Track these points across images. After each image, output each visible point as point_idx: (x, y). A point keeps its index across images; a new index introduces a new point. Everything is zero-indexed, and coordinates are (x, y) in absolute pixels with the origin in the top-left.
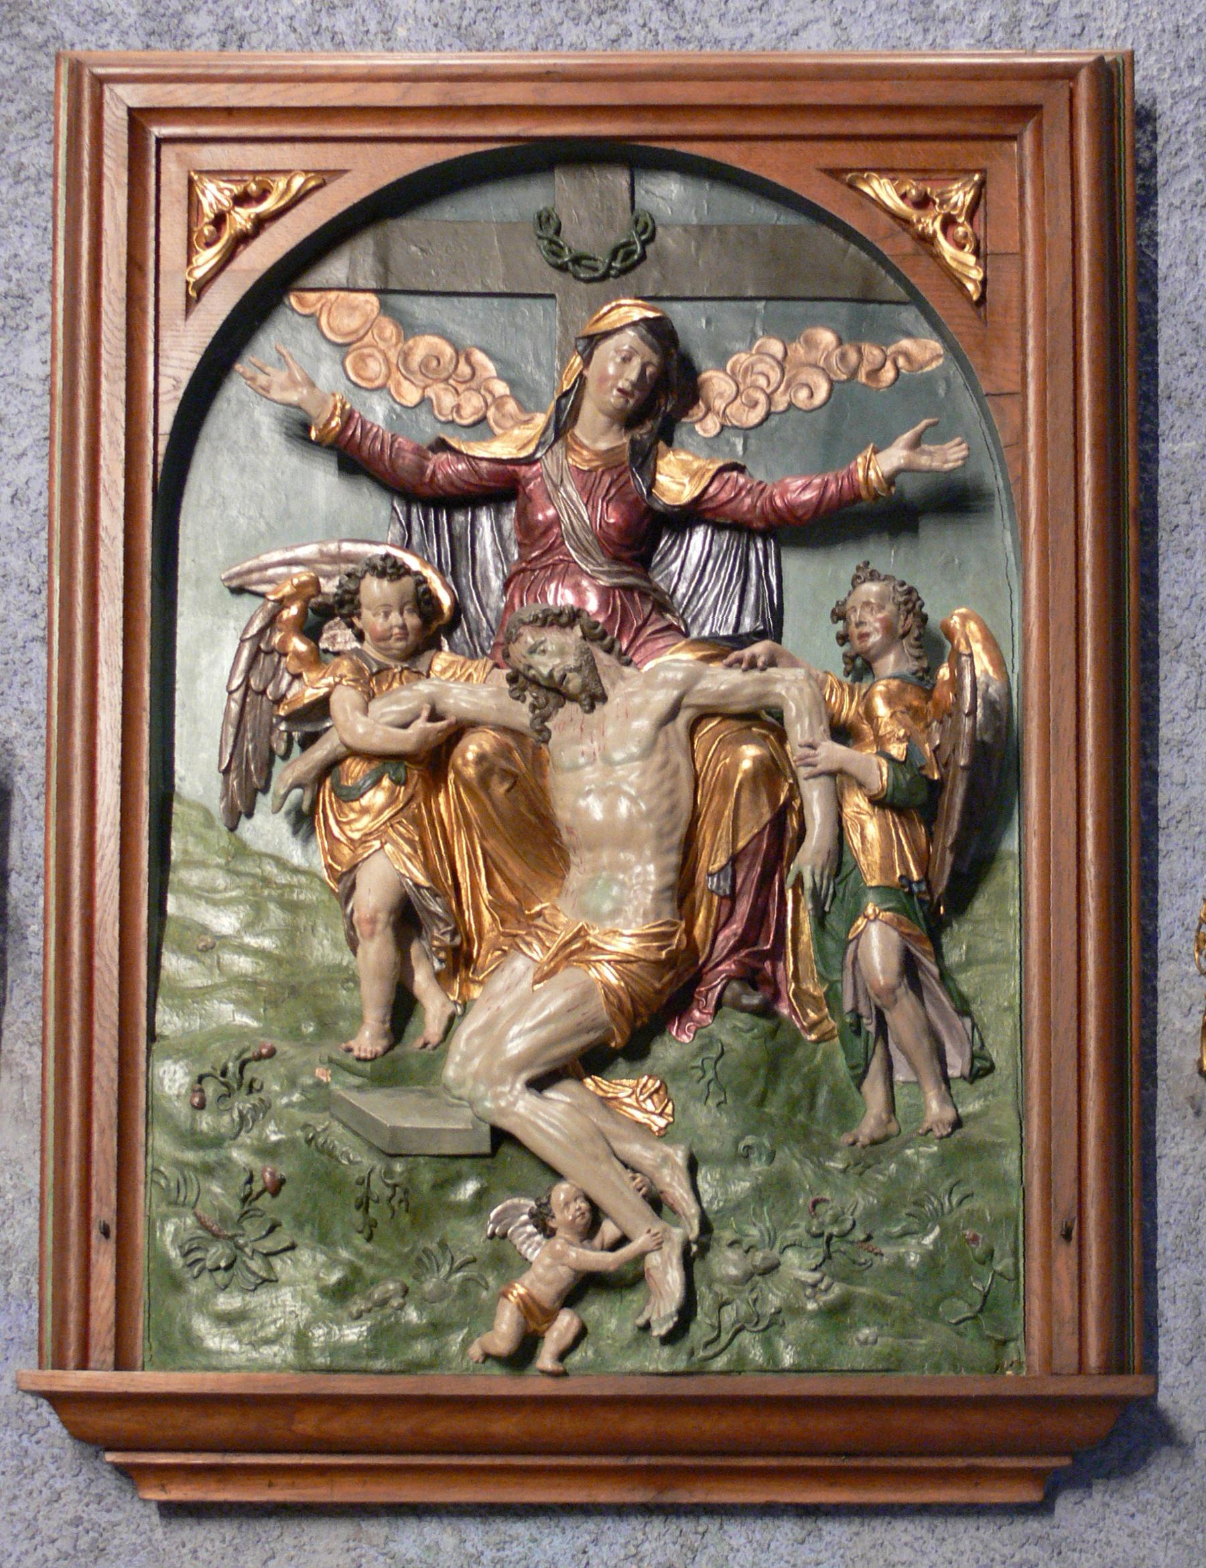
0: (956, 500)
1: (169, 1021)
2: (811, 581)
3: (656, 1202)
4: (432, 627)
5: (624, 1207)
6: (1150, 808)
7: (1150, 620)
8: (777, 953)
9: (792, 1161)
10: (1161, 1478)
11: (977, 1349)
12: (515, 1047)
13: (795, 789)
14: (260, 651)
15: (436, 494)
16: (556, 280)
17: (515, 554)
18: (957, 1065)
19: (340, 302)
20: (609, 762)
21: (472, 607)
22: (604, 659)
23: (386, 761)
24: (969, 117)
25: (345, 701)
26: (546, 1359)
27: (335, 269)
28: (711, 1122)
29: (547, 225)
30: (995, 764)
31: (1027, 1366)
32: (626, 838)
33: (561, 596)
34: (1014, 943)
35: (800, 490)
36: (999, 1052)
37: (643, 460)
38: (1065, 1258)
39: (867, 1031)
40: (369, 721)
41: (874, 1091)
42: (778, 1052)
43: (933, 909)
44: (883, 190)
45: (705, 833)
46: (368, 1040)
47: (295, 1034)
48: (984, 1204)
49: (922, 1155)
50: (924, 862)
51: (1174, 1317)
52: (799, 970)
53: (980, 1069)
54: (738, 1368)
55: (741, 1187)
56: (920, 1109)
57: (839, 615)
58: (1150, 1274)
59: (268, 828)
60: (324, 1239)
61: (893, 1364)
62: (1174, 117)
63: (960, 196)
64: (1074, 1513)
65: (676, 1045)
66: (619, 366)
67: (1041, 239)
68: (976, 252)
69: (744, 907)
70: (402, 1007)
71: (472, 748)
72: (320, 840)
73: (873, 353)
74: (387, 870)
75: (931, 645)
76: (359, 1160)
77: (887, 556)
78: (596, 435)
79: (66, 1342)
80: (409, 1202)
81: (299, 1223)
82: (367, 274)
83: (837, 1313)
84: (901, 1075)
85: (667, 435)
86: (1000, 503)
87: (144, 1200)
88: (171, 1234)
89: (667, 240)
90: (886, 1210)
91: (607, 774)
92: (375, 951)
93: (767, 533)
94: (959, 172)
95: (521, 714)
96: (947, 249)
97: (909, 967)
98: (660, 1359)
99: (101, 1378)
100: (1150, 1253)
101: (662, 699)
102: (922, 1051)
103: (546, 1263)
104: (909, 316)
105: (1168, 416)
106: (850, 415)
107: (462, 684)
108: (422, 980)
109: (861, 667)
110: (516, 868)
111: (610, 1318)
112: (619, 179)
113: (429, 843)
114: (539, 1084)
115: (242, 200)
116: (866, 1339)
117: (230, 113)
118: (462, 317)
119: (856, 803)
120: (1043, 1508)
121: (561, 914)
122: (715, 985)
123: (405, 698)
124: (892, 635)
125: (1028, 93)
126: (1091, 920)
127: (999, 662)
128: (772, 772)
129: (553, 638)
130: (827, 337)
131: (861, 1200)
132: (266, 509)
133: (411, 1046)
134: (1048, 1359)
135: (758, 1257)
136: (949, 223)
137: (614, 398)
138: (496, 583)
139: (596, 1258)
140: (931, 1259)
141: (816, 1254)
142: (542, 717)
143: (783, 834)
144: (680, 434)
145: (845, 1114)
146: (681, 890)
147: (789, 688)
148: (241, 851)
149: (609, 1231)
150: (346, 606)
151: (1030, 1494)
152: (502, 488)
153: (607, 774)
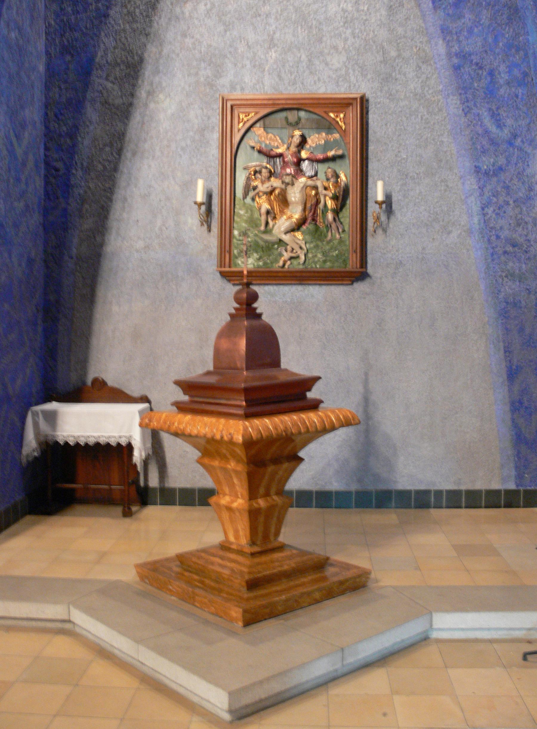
0: (342, 157)
1: (235, 225)
2: (322, 168)
3: (301, 248)
4: (271, 174)
5: (297, 248)
6: (367, 197)
7: (367, 172)
8: (317, 216)
9: (320, 243)
10: (368, 280)
11: (342, 265)
12: (282, 229)
13: (319, 196)
14: (248, 179)
15: (270, 156)
16: (287, 126)
17: (282, 164)
18: (340, 230)
19: (258, 130)
20: (295, 193)
21: (276, 171)
22: (294, 179)
23: (265, 193)
24: (342, 104)
25: (260, 185)
26: (286, 266)
27: (258, 125)
28: (308, 238)
29: (286, 118)
30: (346, 191)
31: (349, 268)
32: (297, 203)
33: (288, 171)
34: (349, 214)
35: (321, 156)
36: (346, 229)
37: (299, 152)
38: (354, 255)
39: (328, 227)
40: (263, 188)
41: (330, 234)
42: (317, 228)
43: (337, 212)
44: (332, 115)
45: (308, 202)
46: (262, 228)
47: (253, 227)
48: (344, 248)
49: (336, 242)
50: (336, 205)
51: (369, 262)
52: (319, 219)
53: (344, 231)
54: (312, 267)
55: (312, 245)
56: (335, 236)
57: (326, 173)
58: (366, 256)
59: (248, 200)
60: (257, 252)
61: (332, 267)
62: (371, 100)
63: (342, 115)
64: (356, 285)
65: (304, 227)
66: (297, 140)
67: (353, 122)
68: (344, 123)
69: (313, 211)
70: (267, 223)
71: (277, 192)
72: (256, 202)
73: (330, 136)
74: (266, 206)
75: (337, 176)
76: (261, 243)
77: (331, 164)
78: (293, 149)
79: (221, 264)
80: (269, 248)
81: (253, 250)
82: (262, 125)
83: (325, 262)
84: (333, 231)
85: (302, 148)
86: (347, 158)
87: (233, 248)
88: (236, 252)
89: (303, 121)
90: (331, 249)
91: (295, 195)
92: (263, 218)
93: (316, 161)
94: (342, 112)
95: (283, 186)
96: (340, 123)
97: (334, 219)
98: (301, 267)
99: (227, 269)
100: (366, 253)
101: (302, 185)
102: (336, 229)
103: (286, 255)
104: (335, 131)
105: (370, 144)
106: (327, 146)
107: (275, 182)
108: (270, 220)
109: (328, 180)
110: (282, 206)
111: (295, 262)
112: (296, 112)
113: (270, 204)
114: (286, 233)
115: (246, 116)
116: (328, 264)
117: (244, 105)
118: (276, 131)
119: (327, 198)
120: (352, 284)
121: (288, 212)
122: (309, 221)
123: (267, 185)
124: (332, 176)
125: (351, 101)
126: (358, 190)
127: (346, 178)
128: (317, 194)
129: (288, 177)
130: (324, 134)
131: (328, 247)
132: (248, 160)
133: (268, 228)
134: (352, 266)
135: (314, 254)
136: (340, 119)
137: (296, 145)
138: (279, 168)
139: (293, 255)
140: (337, 255)
141: (322, 254)
142: (286, 187)
143: (318, 202)
144: (304, 148)
145: (326, 237)
146: (304, 210)
147: (319, 184)
148: (245, 203)
149: (294, 251)
150: (260, 172)
151: (350, 282)
152: (281, 155)
153: (295, 195)
